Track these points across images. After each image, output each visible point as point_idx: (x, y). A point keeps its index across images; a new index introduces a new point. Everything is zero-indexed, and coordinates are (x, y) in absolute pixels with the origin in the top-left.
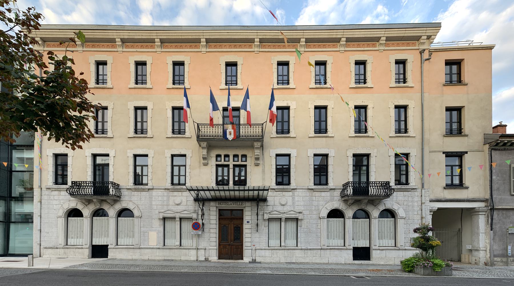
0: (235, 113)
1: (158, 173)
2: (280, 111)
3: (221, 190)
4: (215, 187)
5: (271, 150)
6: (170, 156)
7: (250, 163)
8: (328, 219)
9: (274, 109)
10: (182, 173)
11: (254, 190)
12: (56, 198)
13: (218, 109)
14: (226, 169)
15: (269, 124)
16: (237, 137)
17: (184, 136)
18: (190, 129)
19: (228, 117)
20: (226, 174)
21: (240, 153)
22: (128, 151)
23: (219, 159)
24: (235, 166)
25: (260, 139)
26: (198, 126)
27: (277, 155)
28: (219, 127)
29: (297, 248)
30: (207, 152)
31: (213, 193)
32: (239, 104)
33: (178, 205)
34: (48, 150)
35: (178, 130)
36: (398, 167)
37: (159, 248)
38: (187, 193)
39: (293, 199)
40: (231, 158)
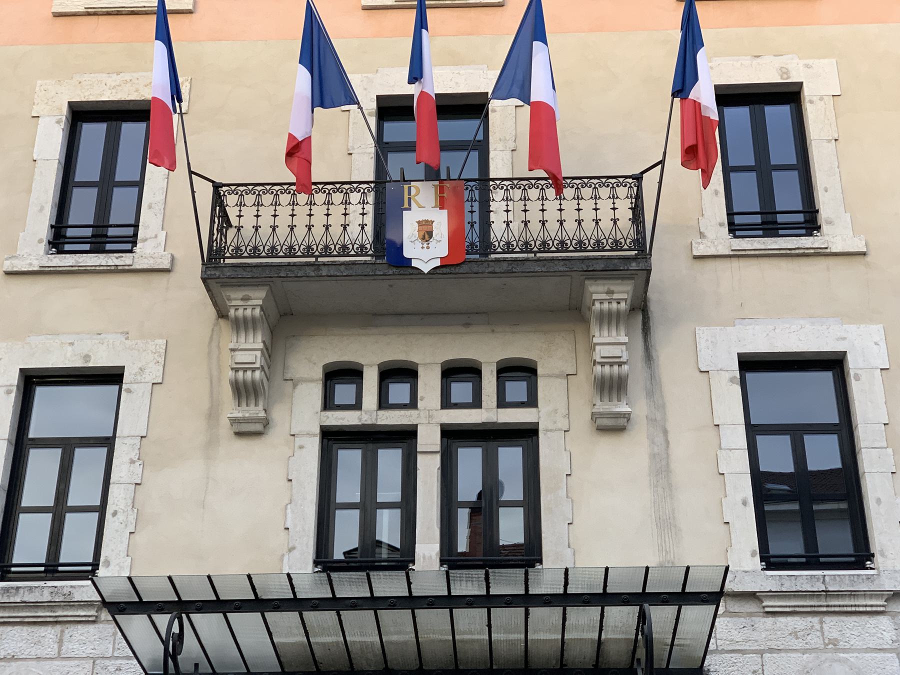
0: (461, 129)
2: (740, 115)
3: (355, 604)
4: (310, 583)
5: (704, 334)
6: (14, 379)
7: (559, 410)
9: (704, 94)
10: (84, 490)
11: (604, 599)
13: (352, 99)
14: (390, 460)
15: (681, 178)
16: (473, 251)
17: (125, 260)
18: (167, 216)
19: (408, 147)
20: (389, 488)
21: (488, 350)
23: (344, 392)
24: (453, 436)
25: (630, 261)
26: (218, 200)
27: (750, 364)
28: (355, 197)
30: (269, 352)
31: (287, 627)
32: (479, 79)
35: (90, 224)
38: (97, 638)
40: (429, 384)
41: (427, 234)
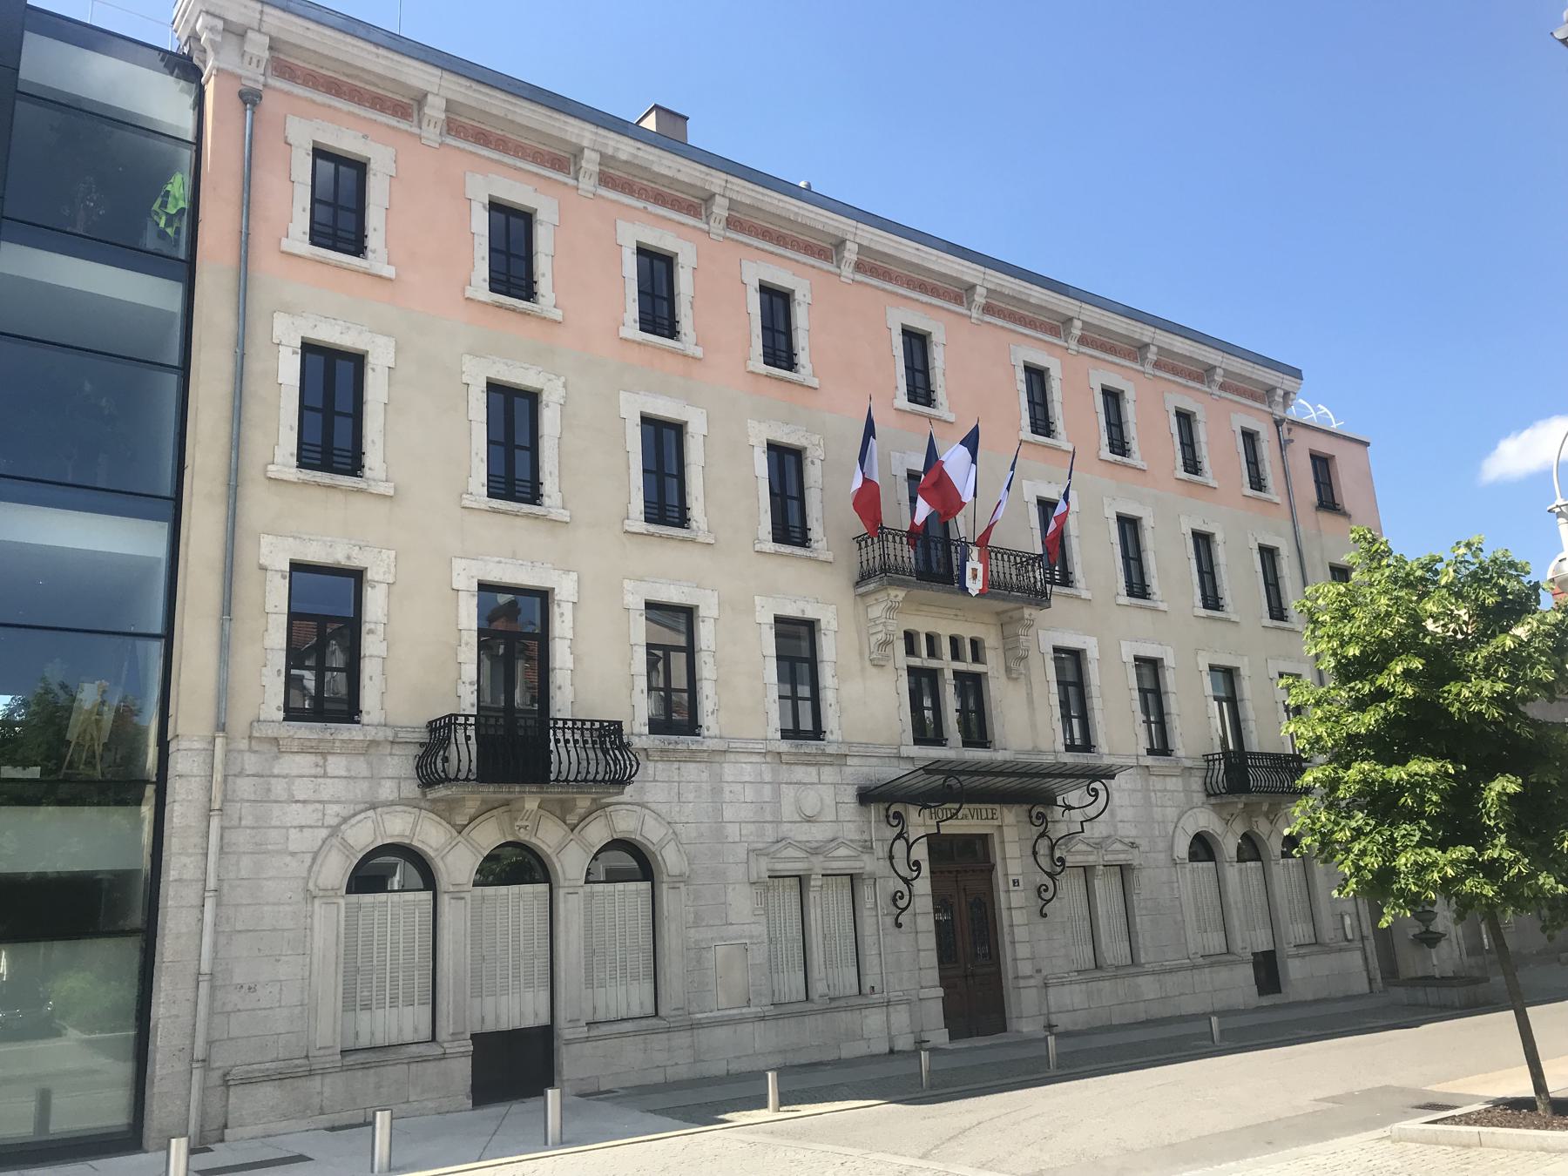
1: (738, 681)
8: (354, 898)
12: (302, 789)
22: (628, 585)
29: (809, 1006)
33: (809, 820)
34: (266, 540)
36: (657, 656)
41: (975, 577)
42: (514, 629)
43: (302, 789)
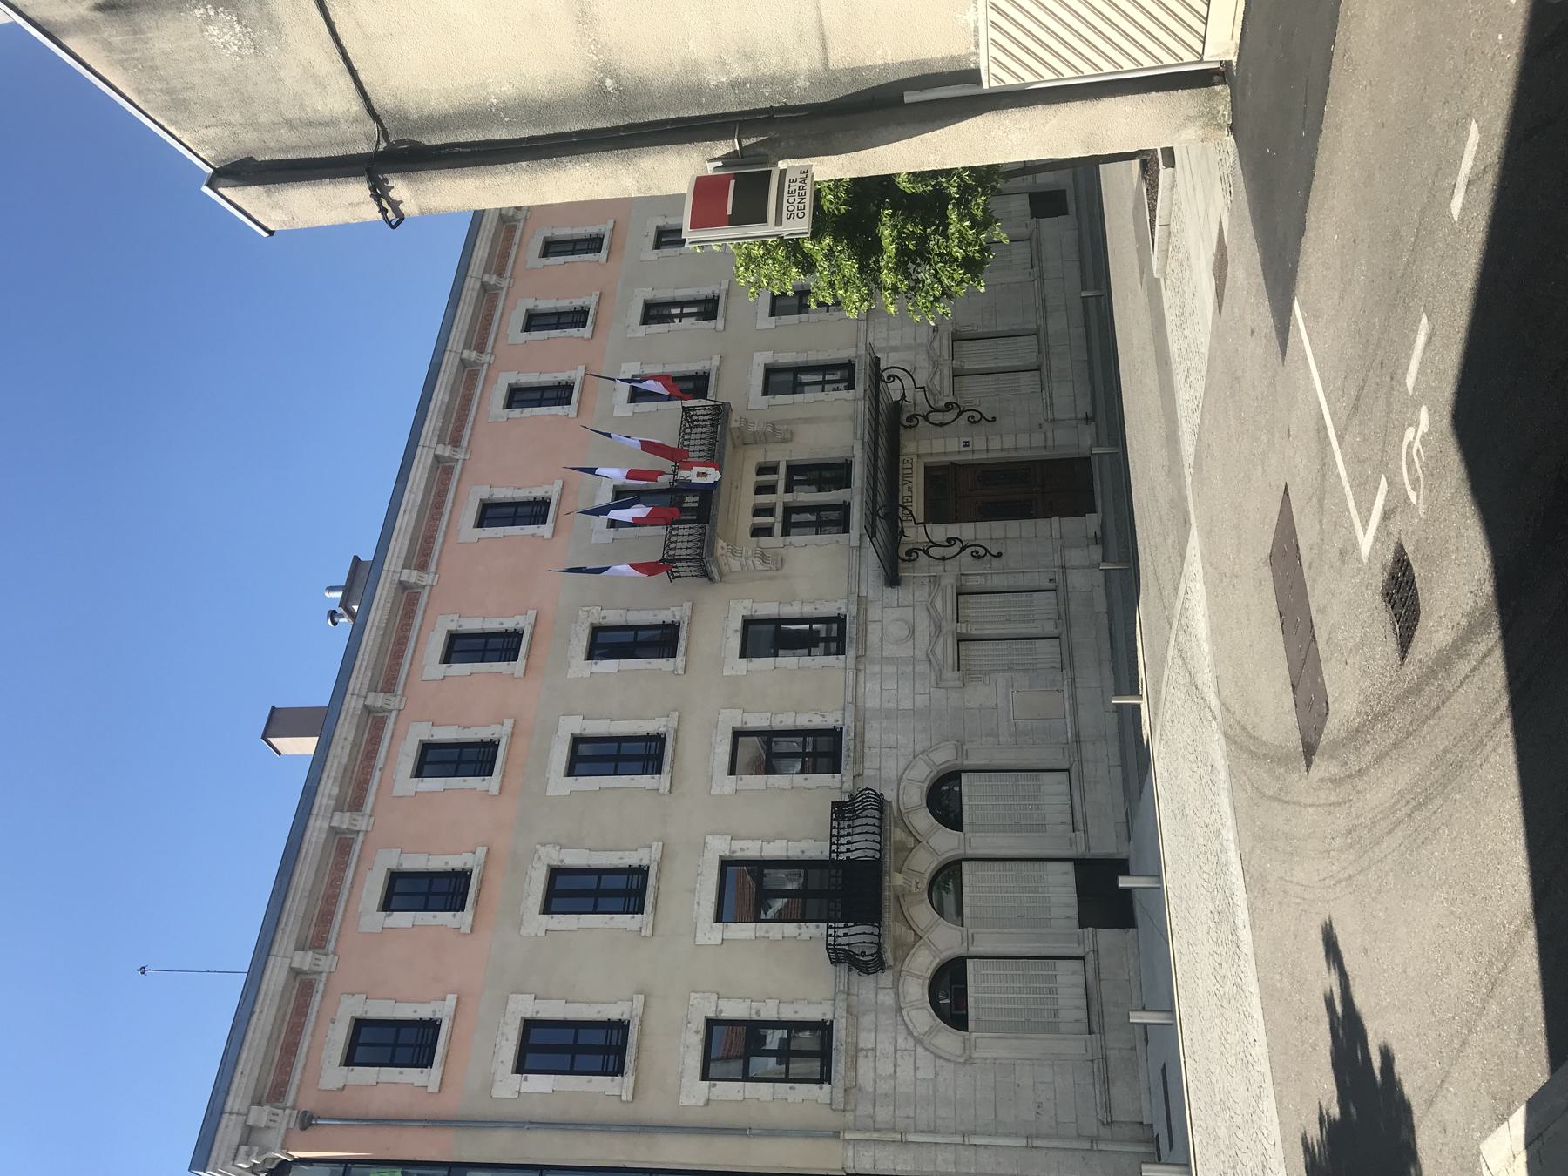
1: (796, 692)
12: (885, 1068)
33: (912, 632)
34: (684, 1101)
35: (661, 640)
37: (1073, 679)
39: (894, 349)
42: (748, 889)
43: (885, 1068)
